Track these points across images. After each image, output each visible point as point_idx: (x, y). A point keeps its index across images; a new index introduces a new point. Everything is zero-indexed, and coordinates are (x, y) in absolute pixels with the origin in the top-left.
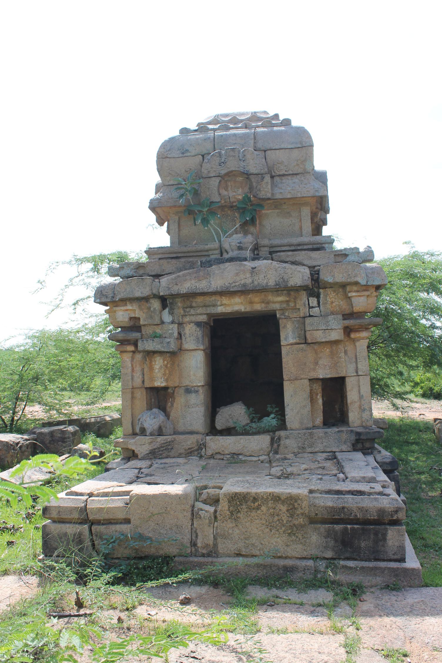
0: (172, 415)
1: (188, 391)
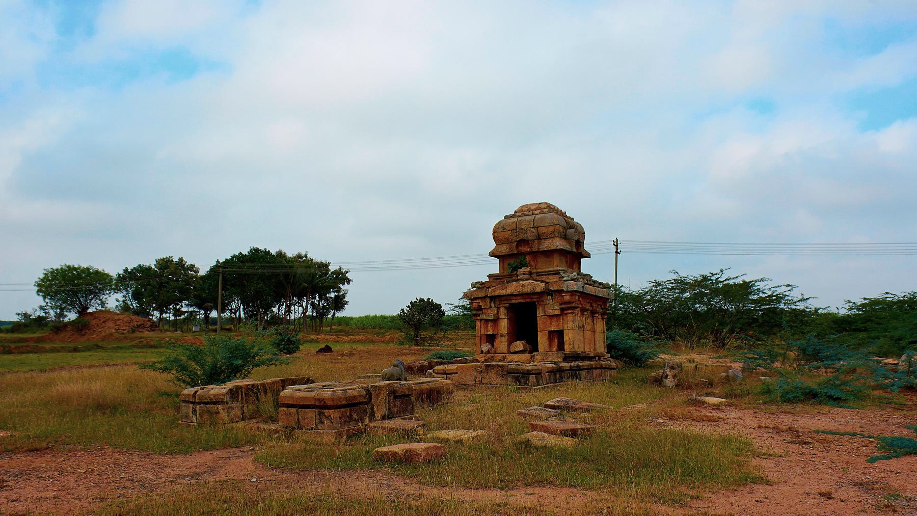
0: (495, 346)
1: (502, 336)
